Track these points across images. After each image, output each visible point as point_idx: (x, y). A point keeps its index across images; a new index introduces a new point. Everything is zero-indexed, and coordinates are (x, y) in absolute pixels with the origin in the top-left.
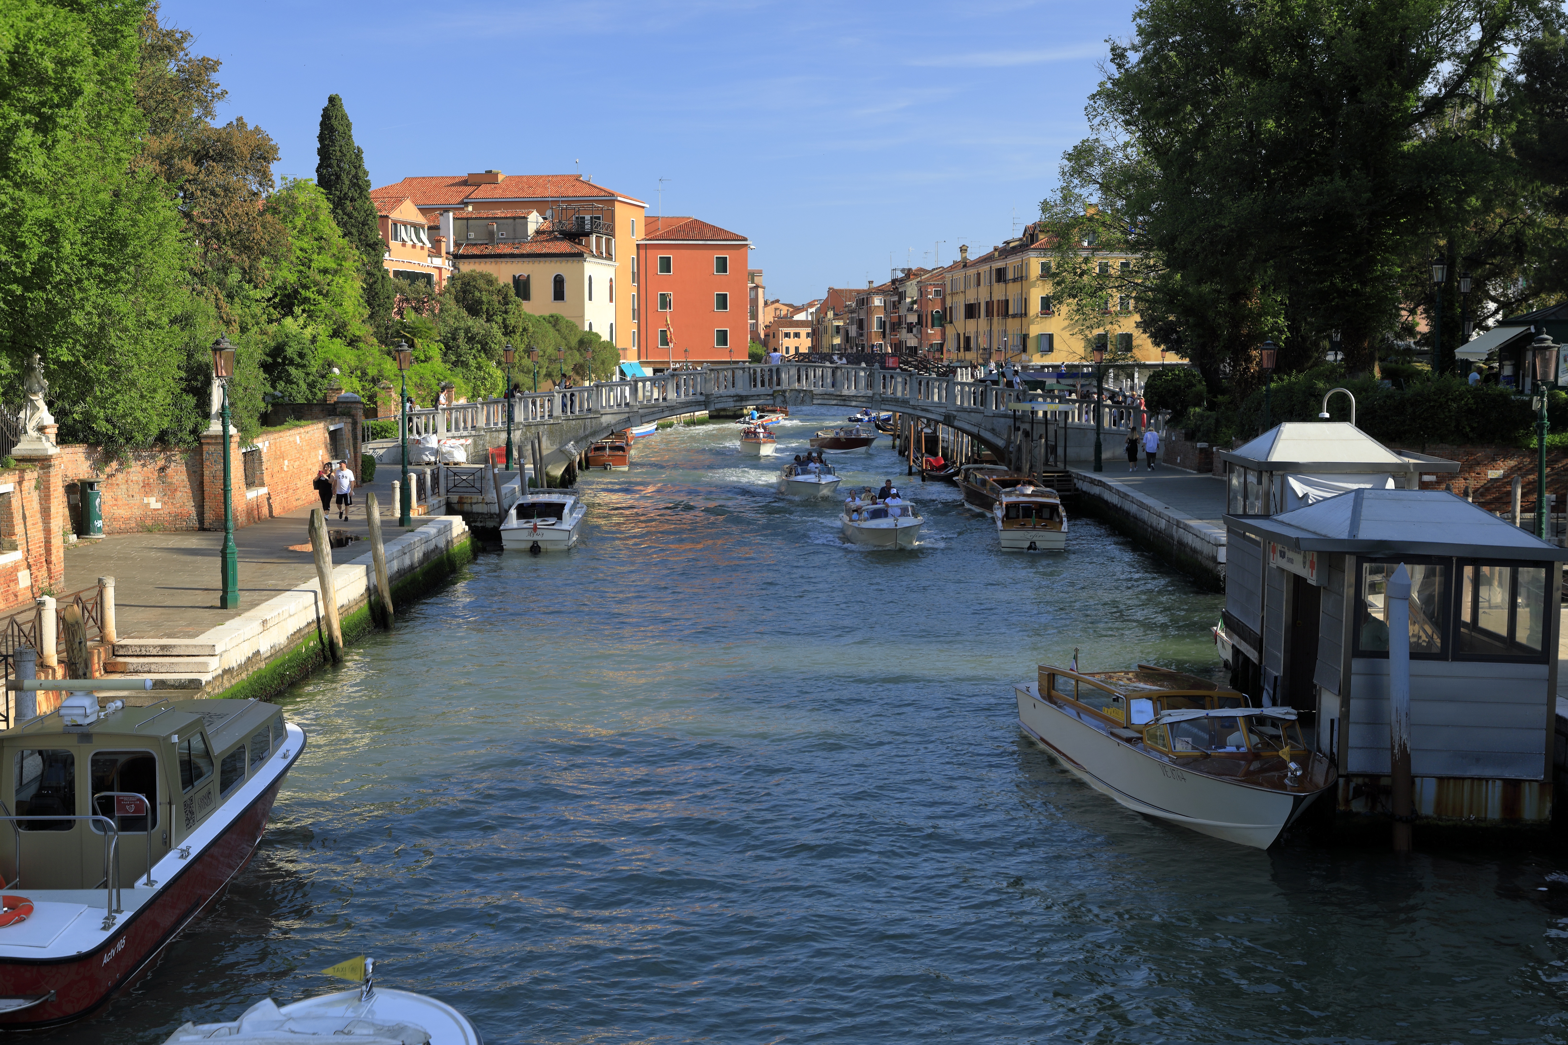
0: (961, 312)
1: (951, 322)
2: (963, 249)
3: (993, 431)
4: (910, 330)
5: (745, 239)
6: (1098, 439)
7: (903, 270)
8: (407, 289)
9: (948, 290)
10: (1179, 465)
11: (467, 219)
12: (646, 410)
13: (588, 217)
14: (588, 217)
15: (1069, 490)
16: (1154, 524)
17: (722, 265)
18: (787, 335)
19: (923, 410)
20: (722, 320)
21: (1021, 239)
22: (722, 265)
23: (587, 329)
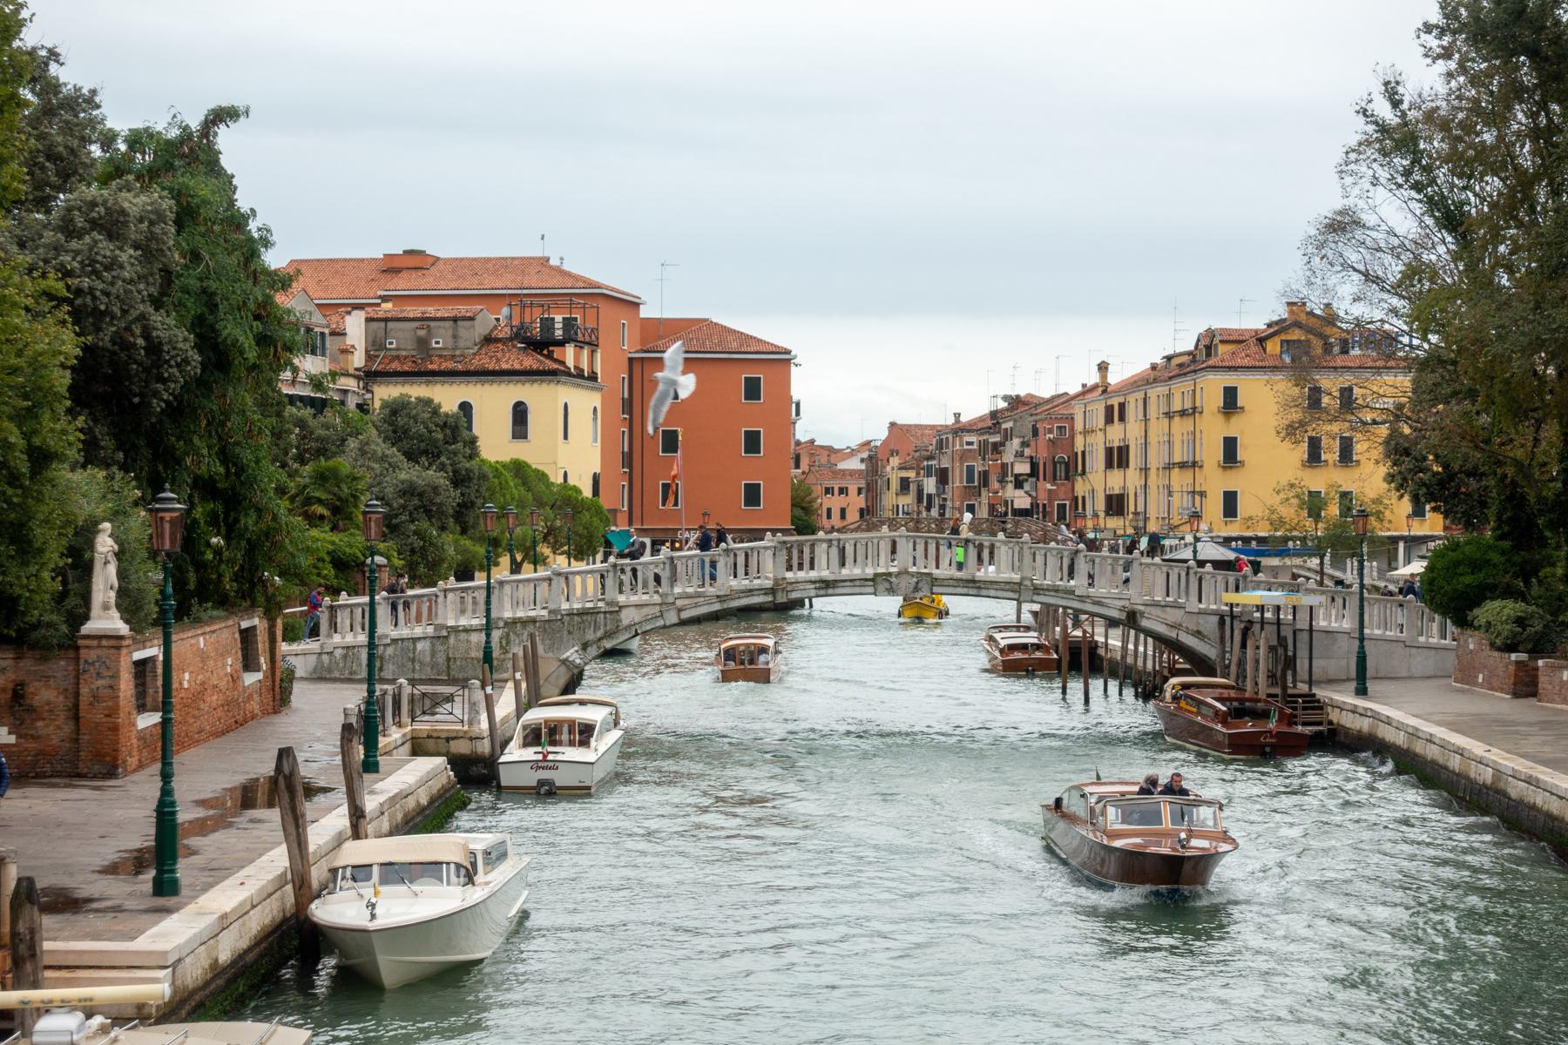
0: (1097, 460)
1: (1084, 472)
2: (1103, 367)
3: (1198, 634)
4: (1019, 484)
5: (788, 352)
6: (1362, 647)
7: (1005, 398)
8: (312, 422)
9: (1079, 426)
10: (1481, 686)
11: (386, 320)
12: (686, 602)
13: (558, 318)
14: (558, 318)
15: (1320, 724)
16: (1472, 775)
17: (753, 390)
18: (828, 491)
19: (1095, 603)
20: (752, 470)
21: (1189, 353)
22: (753, 390)
23: (560, 480)
